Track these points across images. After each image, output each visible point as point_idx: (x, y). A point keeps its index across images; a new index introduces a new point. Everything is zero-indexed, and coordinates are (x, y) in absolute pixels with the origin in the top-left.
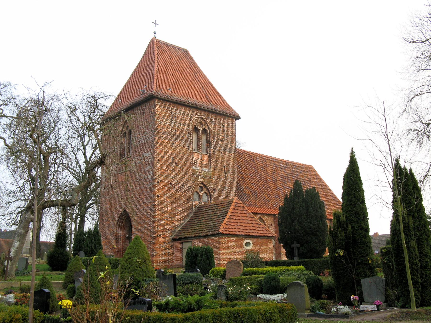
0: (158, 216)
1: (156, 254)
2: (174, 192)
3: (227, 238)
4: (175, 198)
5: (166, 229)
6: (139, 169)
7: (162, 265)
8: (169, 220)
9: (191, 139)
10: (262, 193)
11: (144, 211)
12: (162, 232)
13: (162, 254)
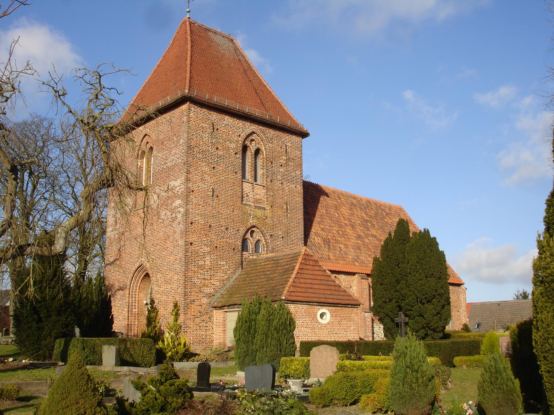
0: (191, 272)
2: (215, 239)
3: (294, 306)
4: (216, 247)
5: (203, 293)
6: (163, 204)
7: (196, 346)
8: (207, 279)
9: (239, 162)
10: (337, 242)
12: (196, 296)
13: (197, 330)
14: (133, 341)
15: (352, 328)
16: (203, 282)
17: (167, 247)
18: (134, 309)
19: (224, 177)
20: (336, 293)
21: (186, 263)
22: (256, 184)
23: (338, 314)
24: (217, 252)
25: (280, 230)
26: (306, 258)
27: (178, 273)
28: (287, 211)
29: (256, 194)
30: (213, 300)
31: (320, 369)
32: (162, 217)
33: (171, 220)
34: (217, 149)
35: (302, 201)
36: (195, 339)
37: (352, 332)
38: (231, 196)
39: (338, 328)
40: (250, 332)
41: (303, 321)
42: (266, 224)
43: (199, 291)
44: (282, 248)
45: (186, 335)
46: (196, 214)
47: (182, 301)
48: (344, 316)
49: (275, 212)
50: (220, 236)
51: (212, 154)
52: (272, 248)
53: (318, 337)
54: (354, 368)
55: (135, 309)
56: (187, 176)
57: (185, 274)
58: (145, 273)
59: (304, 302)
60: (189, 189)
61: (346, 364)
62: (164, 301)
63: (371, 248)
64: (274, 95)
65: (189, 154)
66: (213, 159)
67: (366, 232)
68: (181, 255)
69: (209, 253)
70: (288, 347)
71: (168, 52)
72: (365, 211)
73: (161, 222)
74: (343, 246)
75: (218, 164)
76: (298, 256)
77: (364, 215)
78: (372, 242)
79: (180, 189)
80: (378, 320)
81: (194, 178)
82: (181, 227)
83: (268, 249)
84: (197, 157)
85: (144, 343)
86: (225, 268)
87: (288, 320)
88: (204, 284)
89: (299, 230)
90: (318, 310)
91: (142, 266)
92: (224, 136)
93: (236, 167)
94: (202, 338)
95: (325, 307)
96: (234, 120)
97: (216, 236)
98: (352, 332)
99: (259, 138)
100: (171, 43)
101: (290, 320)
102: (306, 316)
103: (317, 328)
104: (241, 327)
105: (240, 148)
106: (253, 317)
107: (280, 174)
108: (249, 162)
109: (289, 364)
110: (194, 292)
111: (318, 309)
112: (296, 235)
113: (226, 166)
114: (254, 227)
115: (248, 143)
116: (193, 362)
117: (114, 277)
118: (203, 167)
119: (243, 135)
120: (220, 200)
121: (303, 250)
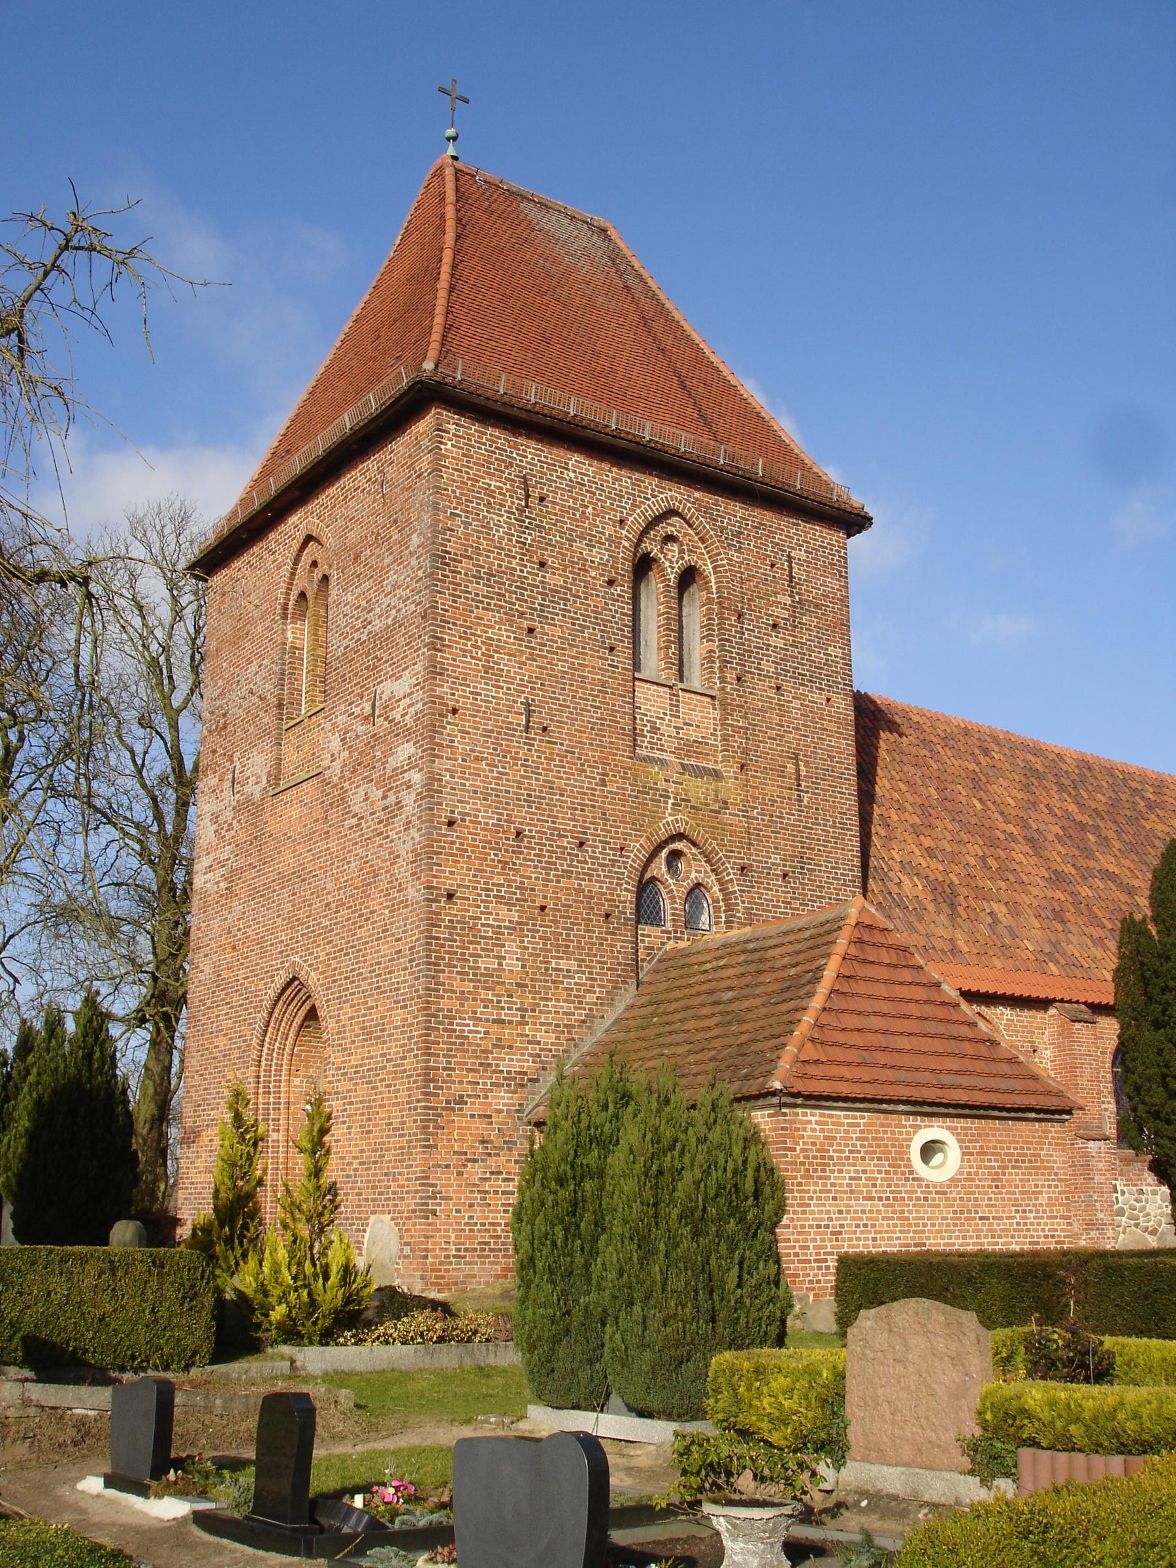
0: (450, 998)
1: (440, 1204)
2: (536, 878)
3: (822, 1115)
4: (543, 908)
5: (495, 1072)
6: (359, 764)
7: (470, 1263)
8: (510, 1022)
9: (622, 614)
10: (981, 894)
11: (380, 975)
12: (469, 1082)
13: (471, 1205)
14: (111, 1262)
15: (1043, 1199)
16: (494, 1033)
17: (371, 912)
18: (274, 1131)
19: (566, 661)
20: (980, 1066)
21: (429, 963)
22: (682, 690)
23: (988, 1148)
24: (547, 926)
25: (776, 848)
26: (866, 938)
27: (404, 1000)
28: (799, 785)
29: (685, 724)
30: (533, 1099)
31: (894, 1423)
32: (355, 809)
33: (381, 815)
34: (542, 564)
35: (852, 750)
36: (467, 1237)
37: (1044, 1211)
38: (593, 729)
39: (990, 1199)
40: (578, 1226)
41: (856, 1171)
42: (723, 830)
43: (481, 1064)
44: (781, 913)
45: (430, 1224)
46: (468, 791)
47: (418, 1101)
48: (1013, 1155)
49: (757, 788)
50: (556, 869)
51: (523, 583)
52: (748, 911)
53: (915, 1232)
54: (1073, 1429)
55: (278, 1131)
56: (432, 659)
57: (428, 1002)
58: (307, 1007)
59: (855, 1100)
60: (440, 704)
61: (1030, 1404)
62: (361, 1102)
63: (1100, 915)
64: (745, 396)
65: (440, 580)
66: (526, 601)
67: (1081, 862)
68: (415, 936)
69: (515, 929)
70: (748, 1301)
71: (389, 270)
72: (1074, 793)
73: (351, 828)
74: (1004, 909)
75: (547, 618)
76: (835, 931)
77: (1072, 808)
78: (1104, 897)
79: (410, 706)
80: (1150, 1169)
81: (458, 667)
82: (413, 838)
83: (734, 916)
84: (468, 592)
85: (163, 1266)
86: (576, 984)
87: (750, 1172)
88: (499, 1039)
89: (843, 849)
90: (915, 1133)
91: (296, 983)
92: (565, 523)
93: (612, 628)
94: (491, 1237)
95: (939, 1121)
96: (601, 469)
97: (542, 868)
98: (1044, 1211)
99: (691, 532)
100: (398, 242)
101: (757, 1170)
102: (866, 1152)
103: (910, 1199)
104: (537, 1204)
105: (623, 564)
106: (591, 1158)
107: (770, 656)
108: (659, 616)
109: (749, 1389)
110: (461, 1070)
111: (911, 1126)
112: (833, 868)
113: (573, 624)
114: (680, 836)
115: (651, 546)
116: (387, 1343)
117: (212, 1023)
118: (490, 627)
119: (637, 521)
120: (555, 743)
121: (853, 912)
